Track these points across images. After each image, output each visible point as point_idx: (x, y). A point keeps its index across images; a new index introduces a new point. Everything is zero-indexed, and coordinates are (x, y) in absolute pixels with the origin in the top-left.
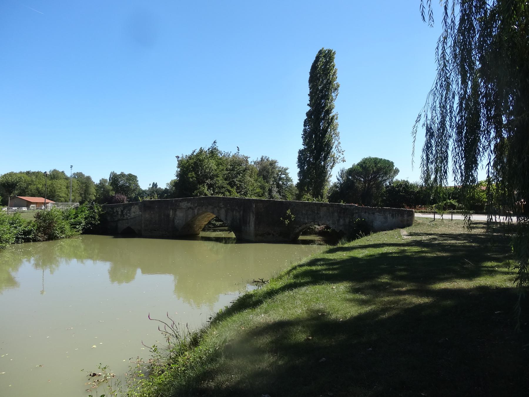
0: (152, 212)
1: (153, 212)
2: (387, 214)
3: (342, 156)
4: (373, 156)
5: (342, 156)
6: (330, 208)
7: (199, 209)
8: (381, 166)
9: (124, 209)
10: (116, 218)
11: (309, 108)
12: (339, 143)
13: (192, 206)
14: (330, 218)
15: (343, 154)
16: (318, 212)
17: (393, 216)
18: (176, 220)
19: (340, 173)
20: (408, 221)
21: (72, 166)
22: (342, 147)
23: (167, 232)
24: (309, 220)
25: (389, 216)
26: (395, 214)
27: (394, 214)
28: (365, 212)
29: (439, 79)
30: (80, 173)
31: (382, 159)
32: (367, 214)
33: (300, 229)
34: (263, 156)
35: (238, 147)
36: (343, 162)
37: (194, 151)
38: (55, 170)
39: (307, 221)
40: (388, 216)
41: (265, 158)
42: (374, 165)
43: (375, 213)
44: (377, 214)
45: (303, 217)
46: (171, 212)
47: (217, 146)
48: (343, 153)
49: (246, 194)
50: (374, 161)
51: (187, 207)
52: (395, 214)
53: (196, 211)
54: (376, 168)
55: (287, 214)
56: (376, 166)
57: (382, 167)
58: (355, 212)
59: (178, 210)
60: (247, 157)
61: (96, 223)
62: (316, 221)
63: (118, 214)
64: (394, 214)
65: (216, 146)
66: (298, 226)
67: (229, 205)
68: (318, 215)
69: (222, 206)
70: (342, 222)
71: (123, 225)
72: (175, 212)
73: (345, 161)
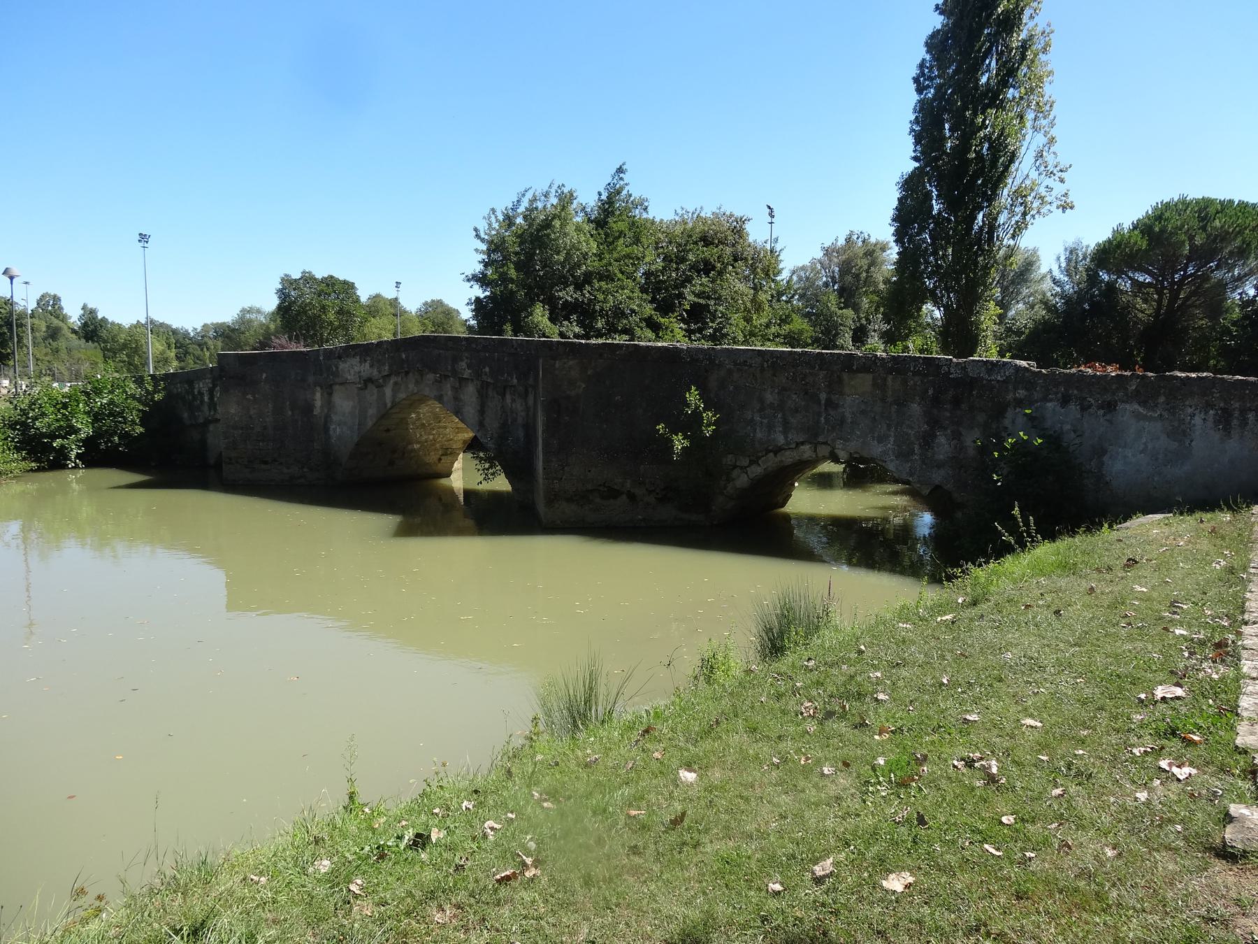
0: (249, 397)
1: (254, 397)
2: (1190, 410)
3: (1059, 189)
4: (1195, 193)
5: (1059, 189)
6: (890, 378)
7: (396, 383)
8: (1222, 227)
10: (200, 413)
11: (938, 21)
12: (1052, 141)
13: (375, 372)
14: (889, 426)
15: (1062, 181)
16: (834, 398)
17: (1224, 421)
18: (333, 427)
19: (1062, 259)
21: (398, 283)
22: (1062, 153)
23: (305, 470)
24: (790, 436)
25: (1200, 423)
26: (1243, 412)
27: (1237, 414)
28: (1065, 401)
30: (438, 301)
31: (1231, 202)
32: (1073, 408)
33: (751, 476)
34: (852, 233)
35: (769, 207)
36: (1064, 208)
38: (378, 296)
39: (781, 440)
40: (1198, 420)
41: (858, 238)
42: (1195, 224)
43: (1120, 406)
44: (1128, 411)
45: (765, 421)
46: (318, 395)
47: (625, 182)
48: (1063, 175)
49: (716, 337)
50: (1200, 211)
51: (360, 377)
52: (1243, 412)
53: (388, 391)
54: (1204, 235)
55: (689, 407)
56: (1204, 228)
57: (1231, 230)
58: (1010, 397)
59: (337, 387)
60: (742, 221)
62: (821, 439)
63: (202, 401)
64: (1237, 414)
65: (622, 183)
66: (745, 462)
67: (487, 369)
68: (832, 413)
69: (467, 373)
70: (943, 445)
72: (330, 394)
73: (1072, 208)
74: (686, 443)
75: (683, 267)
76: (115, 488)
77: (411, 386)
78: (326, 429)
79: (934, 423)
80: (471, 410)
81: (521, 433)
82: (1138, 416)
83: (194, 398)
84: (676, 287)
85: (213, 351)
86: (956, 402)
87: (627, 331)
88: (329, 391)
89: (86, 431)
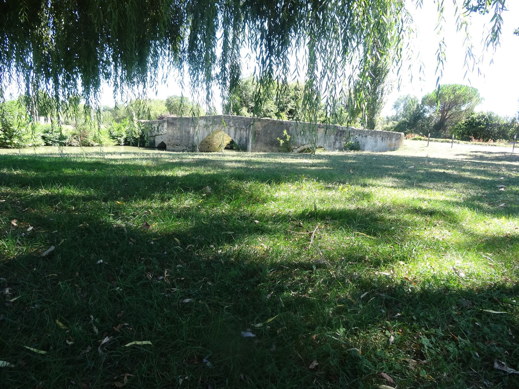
9: (159, 125)
20: (395, 144)
25: (379, 139)
29: (339, 36)
32: (360, 136)
37: (501, 33)
44: (369, 137)
46: (191, 129)
56: (454, 93)
61: (137, 137)
71: (158, 141)
74: (283, 142)
75: (288, 97)
76: (436, 71)
77: (217, 127)
78: (193, 138)
79: (336, 140)
80: (232, 134)
81: (245, 140)
82: (370, 138)
83: (152, 129)
84: (286, 103)
85: (104, 116)
86: (341, 135)
87: (270, 117)
88: (195, 127)
89: (125, 136)
